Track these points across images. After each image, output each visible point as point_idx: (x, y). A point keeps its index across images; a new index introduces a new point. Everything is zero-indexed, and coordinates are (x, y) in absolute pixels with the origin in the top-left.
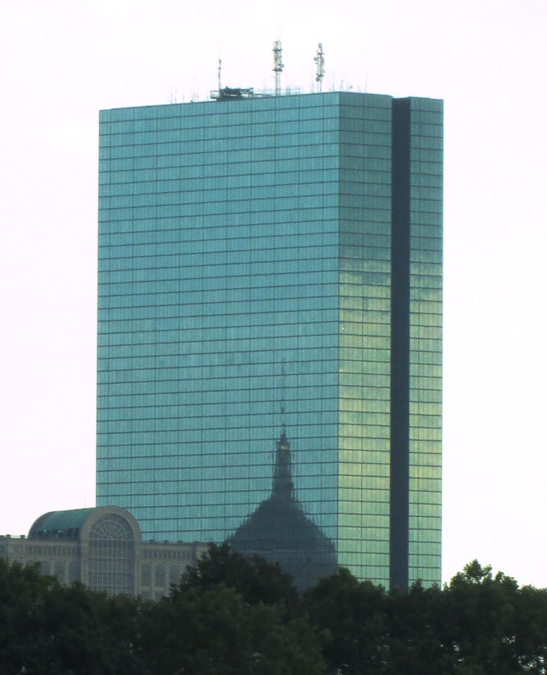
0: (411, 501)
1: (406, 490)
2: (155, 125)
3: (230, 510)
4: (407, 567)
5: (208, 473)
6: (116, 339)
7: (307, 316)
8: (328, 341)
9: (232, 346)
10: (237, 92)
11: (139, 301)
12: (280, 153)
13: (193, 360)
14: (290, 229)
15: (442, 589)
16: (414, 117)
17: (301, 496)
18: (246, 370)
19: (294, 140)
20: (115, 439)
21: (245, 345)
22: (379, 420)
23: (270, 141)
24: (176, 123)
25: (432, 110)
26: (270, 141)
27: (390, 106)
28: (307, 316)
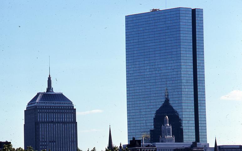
0: (197, 37)
1: (198, 123)
2: (137, 18)
3: (157, 103)
4: (198, 97)
5: (152, 95)
6: (130, 67)
7: (174, 59)
8: (178, 64)
9: (156, 66)
10: (156, 10)
11: (135, 58)
12: (167, 22)
13: (148, 70)
14: (169, 39)
15: (212, 145)
16: (196, 13)
17: (170, 102)
18: (160, 72)
19: (170, 19)
20: (131, 89)
21: (160, 66)
22: (202, 65)
23: (164, 20)
24: (143, 17)
25: (201, 11)
26: (164, 20)
27: (191, 10)
28: (174, 59)
